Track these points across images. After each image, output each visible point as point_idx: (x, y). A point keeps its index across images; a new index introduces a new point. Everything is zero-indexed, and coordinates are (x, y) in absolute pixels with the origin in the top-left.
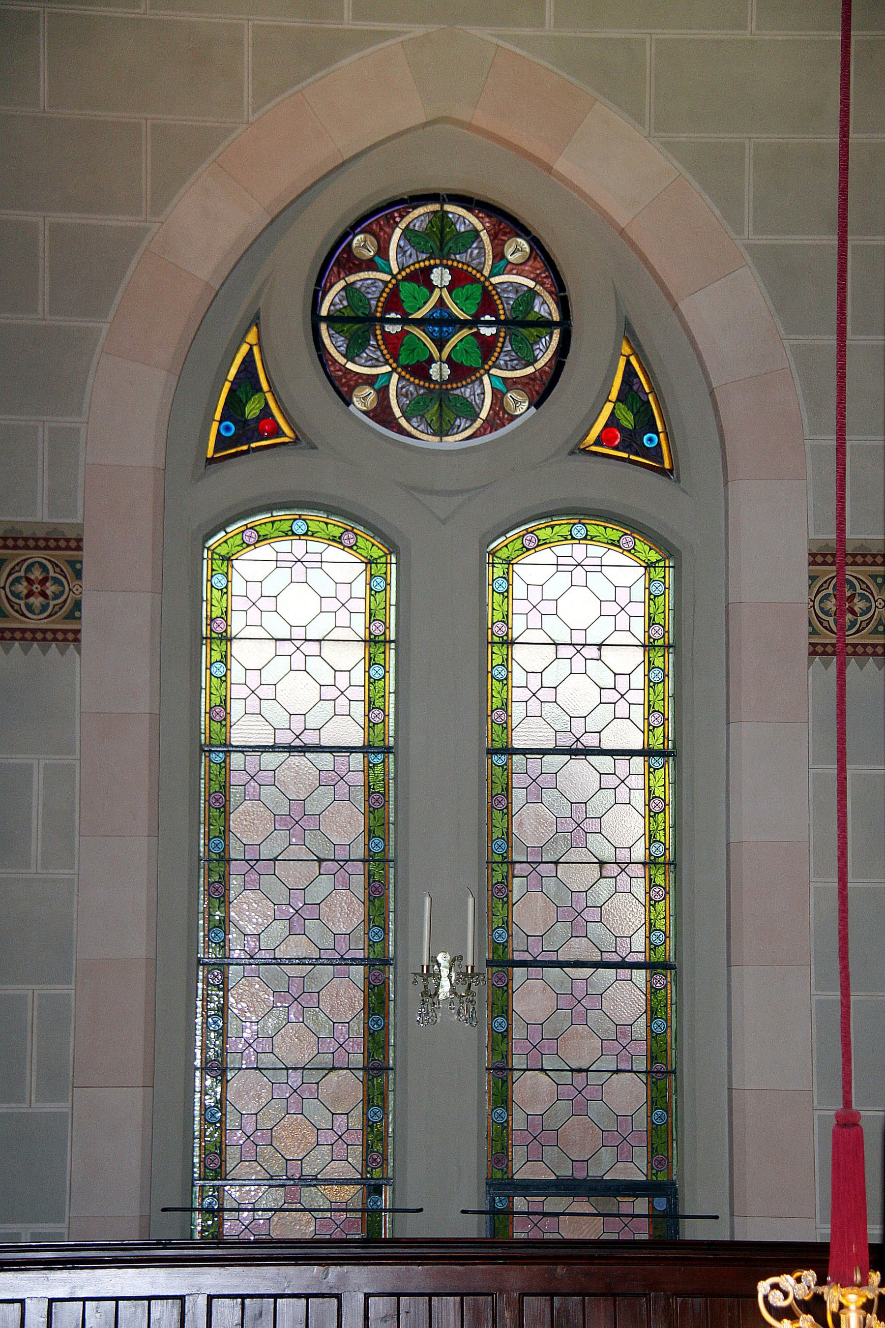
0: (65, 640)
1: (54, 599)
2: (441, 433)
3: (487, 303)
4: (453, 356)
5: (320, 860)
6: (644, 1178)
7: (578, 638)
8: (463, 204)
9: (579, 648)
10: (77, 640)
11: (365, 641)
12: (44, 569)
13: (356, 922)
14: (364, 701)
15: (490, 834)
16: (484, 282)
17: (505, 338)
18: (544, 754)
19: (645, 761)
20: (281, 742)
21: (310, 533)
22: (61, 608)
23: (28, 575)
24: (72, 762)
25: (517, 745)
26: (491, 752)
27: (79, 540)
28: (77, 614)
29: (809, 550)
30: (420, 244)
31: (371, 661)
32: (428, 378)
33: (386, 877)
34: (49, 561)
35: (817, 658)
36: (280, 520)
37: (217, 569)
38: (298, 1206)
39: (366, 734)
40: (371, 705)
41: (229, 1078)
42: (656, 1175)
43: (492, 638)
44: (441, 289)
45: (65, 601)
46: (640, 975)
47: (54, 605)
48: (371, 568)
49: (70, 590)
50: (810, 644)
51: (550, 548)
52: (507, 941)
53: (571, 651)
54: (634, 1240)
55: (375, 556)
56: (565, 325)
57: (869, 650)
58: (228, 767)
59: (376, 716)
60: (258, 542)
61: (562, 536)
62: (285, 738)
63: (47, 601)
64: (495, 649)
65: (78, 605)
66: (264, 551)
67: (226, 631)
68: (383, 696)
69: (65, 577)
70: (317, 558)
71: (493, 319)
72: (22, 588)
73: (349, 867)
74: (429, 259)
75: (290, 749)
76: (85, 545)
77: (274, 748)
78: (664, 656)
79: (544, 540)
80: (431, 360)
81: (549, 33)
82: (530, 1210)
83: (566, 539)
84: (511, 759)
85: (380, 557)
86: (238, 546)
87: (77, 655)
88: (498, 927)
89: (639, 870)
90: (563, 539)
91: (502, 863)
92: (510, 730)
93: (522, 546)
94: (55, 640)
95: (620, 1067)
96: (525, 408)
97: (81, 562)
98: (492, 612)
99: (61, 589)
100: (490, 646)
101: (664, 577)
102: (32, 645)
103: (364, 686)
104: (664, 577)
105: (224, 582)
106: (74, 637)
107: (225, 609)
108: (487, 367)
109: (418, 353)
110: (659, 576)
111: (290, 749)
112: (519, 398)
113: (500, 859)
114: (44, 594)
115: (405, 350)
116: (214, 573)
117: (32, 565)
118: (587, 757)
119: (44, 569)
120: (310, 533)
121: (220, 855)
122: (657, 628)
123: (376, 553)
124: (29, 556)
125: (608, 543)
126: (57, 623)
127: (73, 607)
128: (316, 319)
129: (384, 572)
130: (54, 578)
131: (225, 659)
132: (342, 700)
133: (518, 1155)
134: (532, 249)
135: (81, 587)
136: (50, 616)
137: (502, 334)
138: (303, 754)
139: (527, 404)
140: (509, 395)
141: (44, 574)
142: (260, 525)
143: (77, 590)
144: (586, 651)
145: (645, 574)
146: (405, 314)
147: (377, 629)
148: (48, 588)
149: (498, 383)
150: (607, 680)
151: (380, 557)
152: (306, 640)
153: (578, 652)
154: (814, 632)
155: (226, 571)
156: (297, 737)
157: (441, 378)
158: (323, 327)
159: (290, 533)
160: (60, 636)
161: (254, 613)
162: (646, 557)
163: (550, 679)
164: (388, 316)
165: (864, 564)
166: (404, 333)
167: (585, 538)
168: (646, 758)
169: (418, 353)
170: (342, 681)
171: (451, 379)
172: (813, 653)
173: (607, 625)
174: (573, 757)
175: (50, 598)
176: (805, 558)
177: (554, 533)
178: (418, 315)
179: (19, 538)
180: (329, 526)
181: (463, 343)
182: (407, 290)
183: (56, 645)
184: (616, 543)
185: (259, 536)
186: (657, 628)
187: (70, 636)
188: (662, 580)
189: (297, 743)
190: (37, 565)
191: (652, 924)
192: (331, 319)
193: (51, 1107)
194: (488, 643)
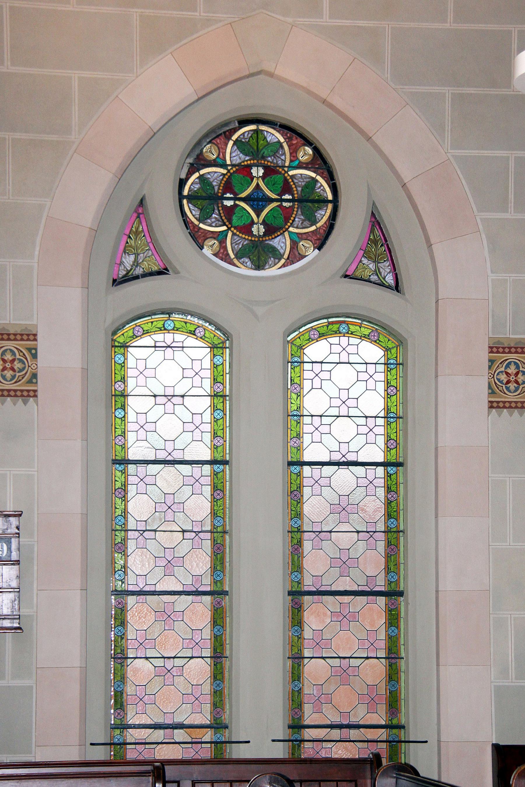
0: (16, 396)
1: (19, 372)
2: (258, 267)
3: (286, 188)
4: (266, 220)
5: (184, 531)
6: (209, 723)
7: (169, 392)
8: (272, 126)
9: (169, 398)
10: (35, 396)
11: (211, 396)
12: (13, 353)
13: (205, 568)
14: (128, 431)
15: (113, 513)
16: (284, 174)
17: (297, 208)
18: (148, 464)
19: (384, 469)
20: (333, 459)
21: (175, 329)
22: (23, 378)
23: (3, 357)
24: (33, 473)
25: (131, 457)
26: (291, 464)
27: (35, 335)
28: (34, 381)
29: (489, 344)
30: (245, 150)
31: (214, 408)
32: (250, 233)
33: (224, 541)
34: (17, 348)
35: (494, 410)
36: (157, 321)
37: (295, 354)
38: (173, 741)
39: (386, 455)
40: (215, 435)
41: (128, 664)
42: (391, 720)
43: (115, 392)
44: (258, 178)
45: (26, 373)
46: (207, 599)
47: (19, 376)
48: (214, 351)
49: (29, 366)
50: (489, 402)
51: (150, 336)
52: (124, 579)
53: (164, 400)
54: (331, 758)
55: (216, 343)
56: (335, 202)
57: (19, 393)
58: (302, 475)
59: (218, 442)
60: (143, 334)
61: (158, 328)
62: (336, 457)
63: (15, 373)
64: (117, 399)
65: (490, 367)
66: (147, 341)
67: (124, 390)
68: (223, 429)
69: (495, 383)
70: (180, 345)
71: (232, 196)
72: (17, 365)
73: (201, 535)
74: (250, 160)
75: (338, 464)
76: (39, 337)
77: (330, 463)
78: (223, 402)
79: (146, 331)
80: (252, 223)
81: (137, 10)
82: (406, 740)
83: (161, 330)
84: (127, 467)
85: (219, 344)
86: (130, 337)
87: (36, 407)
88: (118, 570)
89: (382, 536)
90: (159, 330)
91: (121, 531)
92: (126, 448)
93: (133, 334)
94: (9, 396)
95: (369, 656)
96: (312, 251)
97: (489, 393)
98: (115, 376)
99: (23, 366)
100: (113, 397)
101: (396, 357)
102: (7, 399)
103: (128, 422)
104: (396, 357)
105: (122, 359)
106: (491, 349)
107: (123, 376)
108: (287, 227)
109: (244, 219)
110: (220, 353)
111: (338, 464)
112: (307, 245)
113: (120, 528)
114: (13, 369)
115: (236, 216)
116: (116, 354)
117: (6, 350)
118: (349, 467)
119: (13, 353)
120: (350, 332)
121: (121, 527)
122: (219, 385)
123: (390, 345)
124: (5, 345)
125: (187, 332)
126: (22, 386)
127: (31, 377)
128: (181, 197)
129: (395, 356)
130: (19, 359)
131: (123, 407)
132: (317, 433)
133: (307, 709)
134: (314, 153)
135: (36, 365)
136: (16, 382)
137: (296, 206)
138: (346, 467)
139: (312, 248)
140: (301, 243)
141: (13, 357)
142: (144, 324)
143: (34, 367)
144: (174, 400)
145: (385, 355)
146: (235, 194)
147: (219, 388)
148: (15, 365)
149: (294, 237)
150: (188, 417)
151: (219, 344)
152: (174, 396)
153: (169, 400)
154: (492, 393)
155: (123, 352)
156: (344, 456)
157: (258, 234)
158: (185, 201)
159: (163, 329)
160: (12, 393)
161: (141, 378)
162: (386, 345)
163: (151, 417)
164: (225, 196)
165: (22, 340)
166: (236, 206)
167: (173, 329)
168: (385, 468)
169: (244, 219)
170: (197, 420)
171: (265, 234)
172: (491, 407)
173: (187, 383)
174: (166, 465)
175: (17, 371)
176: (487, 350)
177: (329, 329)
178: (243, 195)
179: (30, 334)
180: (187, 324)
181: (272, 212)
182: (237, 179)
183: (22, 399)
184: (193, 332)
185: (144, 331)
186: (219, 385)
187: (32, 394)
188: (395, 359)
189: (344, 459)
190: (8, 351)
191: (388, 568)
192: (191, 198)
193: (18, 683)
194: (112, 395)
